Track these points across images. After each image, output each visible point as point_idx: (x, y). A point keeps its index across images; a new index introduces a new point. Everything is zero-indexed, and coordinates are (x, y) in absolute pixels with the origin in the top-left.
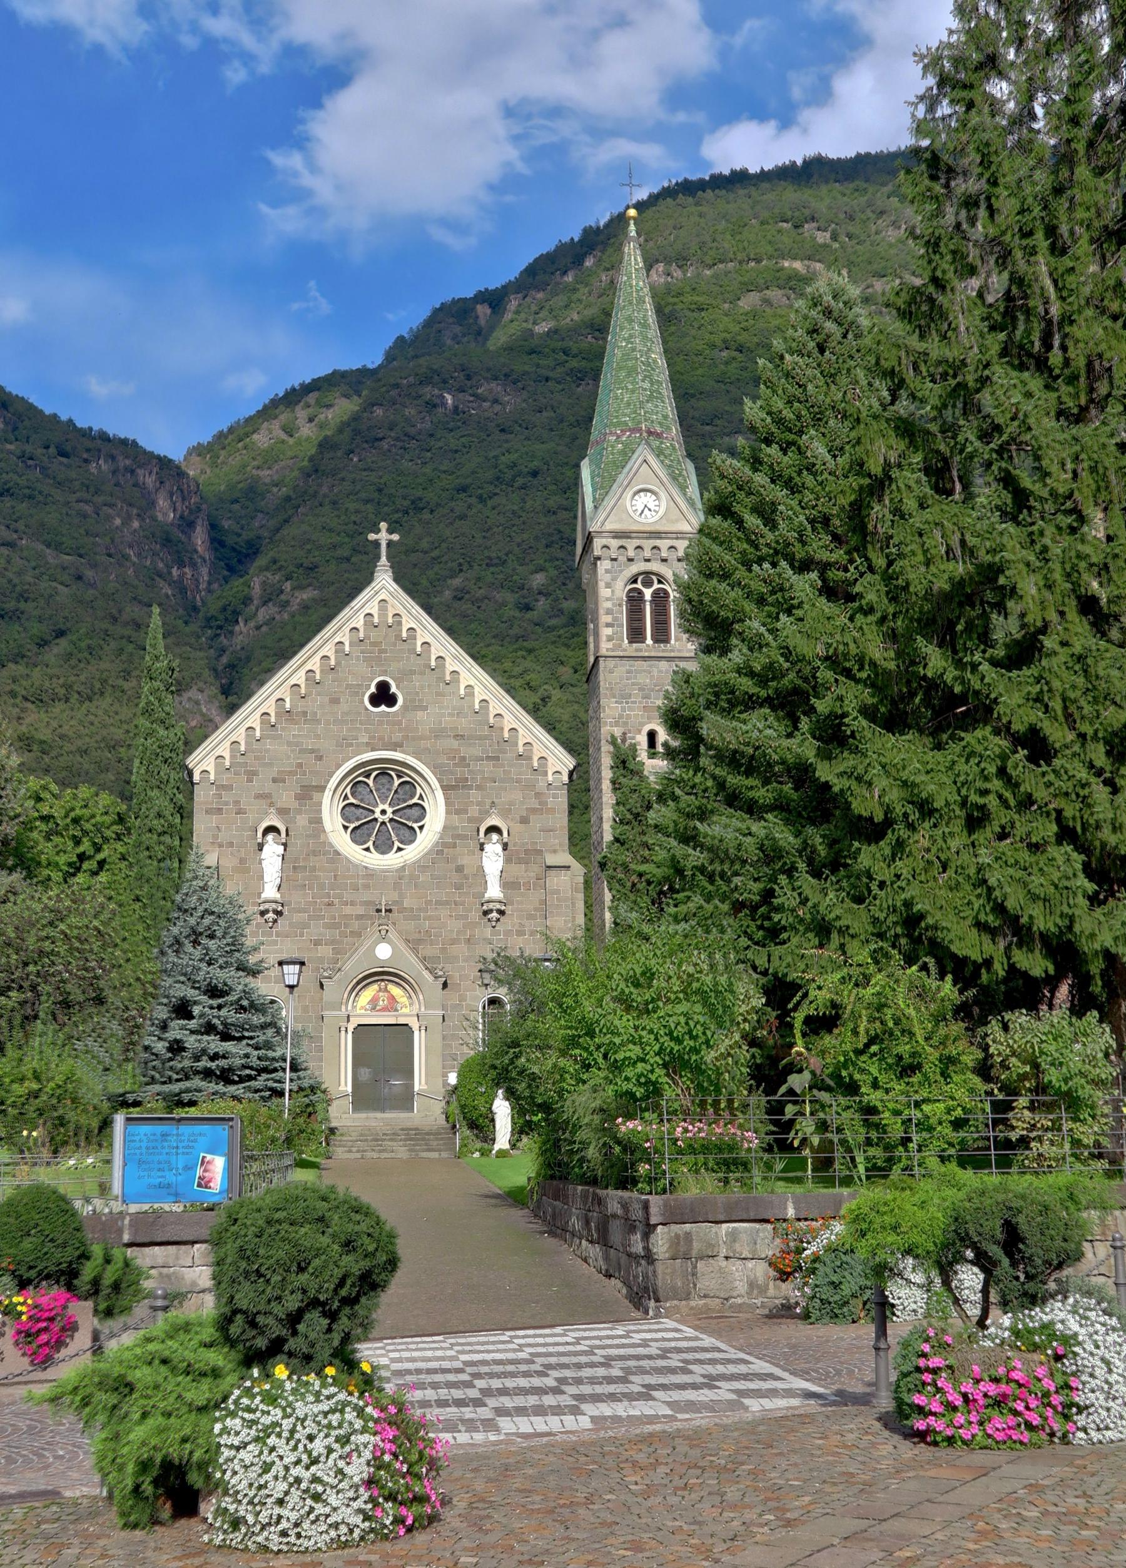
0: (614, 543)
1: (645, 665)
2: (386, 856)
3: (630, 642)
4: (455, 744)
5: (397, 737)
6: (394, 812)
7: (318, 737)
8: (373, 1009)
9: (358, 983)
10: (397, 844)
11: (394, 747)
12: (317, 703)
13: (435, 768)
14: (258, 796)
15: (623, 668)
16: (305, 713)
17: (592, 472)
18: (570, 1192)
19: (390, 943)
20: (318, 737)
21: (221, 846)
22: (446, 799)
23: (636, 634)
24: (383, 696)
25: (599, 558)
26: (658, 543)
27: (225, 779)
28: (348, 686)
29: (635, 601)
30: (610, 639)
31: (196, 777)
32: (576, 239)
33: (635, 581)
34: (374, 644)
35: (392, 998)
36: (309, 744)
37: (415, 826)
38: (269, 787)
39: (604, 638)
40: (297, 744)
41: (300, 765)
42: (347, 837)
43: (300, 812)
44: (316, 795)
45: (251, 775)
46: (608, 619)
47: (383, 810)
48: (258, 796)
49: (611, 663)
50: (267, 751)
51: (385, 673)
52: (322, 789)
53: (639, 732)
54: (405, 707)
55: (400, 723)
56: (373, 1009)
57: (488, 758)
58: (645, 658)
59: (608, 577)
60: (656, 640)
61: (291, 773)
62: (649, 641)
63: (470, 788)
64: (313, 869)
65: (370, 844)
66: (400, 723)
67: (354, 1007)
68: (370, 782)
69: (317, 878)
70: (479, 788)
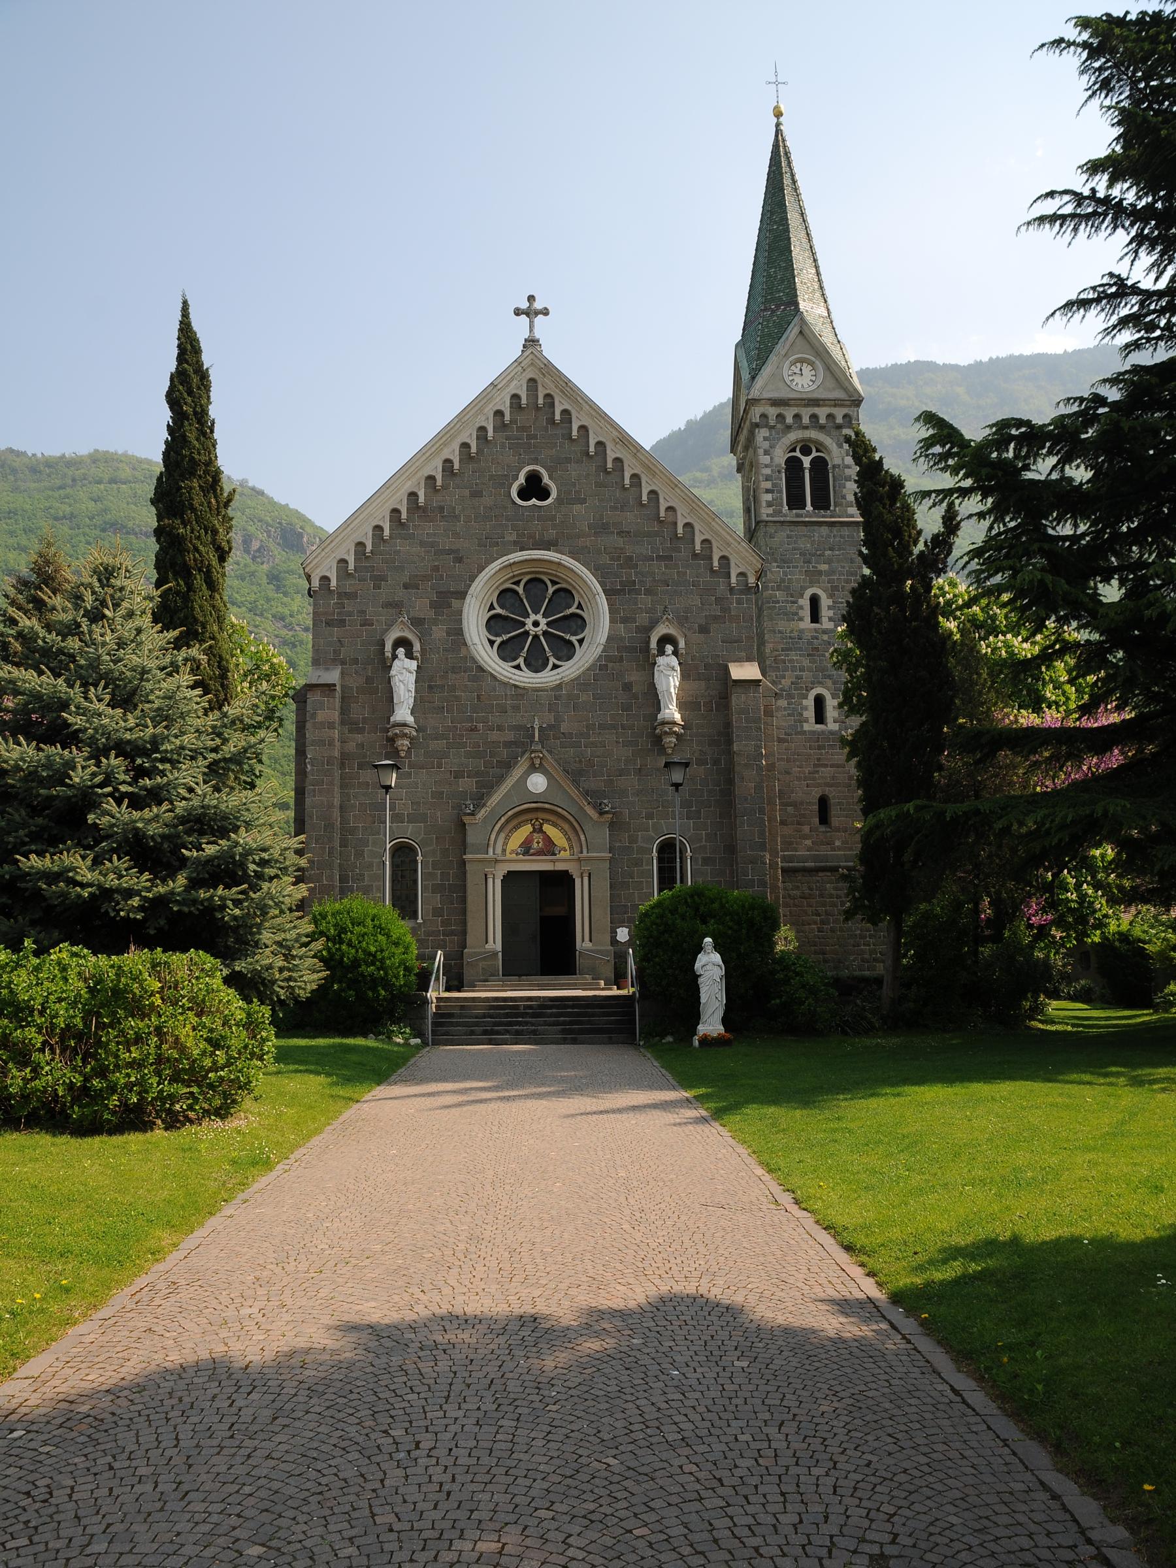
0: (772, 412)
1: (803, 530)
4: (620, 542)
5: (552, 533)
6: (548, 624)
7: (456, 535)
8: (526, 853)
9: (507, 821)
10: (552, 660)
13: (597, 570)
14: (388, 605)
15: (782, 535)
16: (441, 509)
19: (545, 772)
20: (456, 535)
21: (343, 663)
23: (796, 501)
24: (534, 488)
26: (816, 410)
27: (349, 586)
28: (491, 477)
29: (793, 466)
30: (769, 504)
33: (794, 450)
34: (522, 429)
35: (549, 841)
38: (400, 594)
40: (432, 545)
41: (436, 569)
43: (435, 622)
44: (455, 603)
45: (378, 580)
46: (768, 485)
47: (536, 623)
48: (388, 605)
51: (535, 461)
52: (462, 595)
53: (802, 596)
54: (558, 499)
55: (553, 518)
57: (659, 558)
58: (806, 524)
59: (766, 445)
61: (426, 578)
62: (809, 507)
63: (638, 592)
65: (521, 661)
66: (553, 518)
67: (504, 851)
68: (520, 590)
69: (458, 698)
70: (648, 592)
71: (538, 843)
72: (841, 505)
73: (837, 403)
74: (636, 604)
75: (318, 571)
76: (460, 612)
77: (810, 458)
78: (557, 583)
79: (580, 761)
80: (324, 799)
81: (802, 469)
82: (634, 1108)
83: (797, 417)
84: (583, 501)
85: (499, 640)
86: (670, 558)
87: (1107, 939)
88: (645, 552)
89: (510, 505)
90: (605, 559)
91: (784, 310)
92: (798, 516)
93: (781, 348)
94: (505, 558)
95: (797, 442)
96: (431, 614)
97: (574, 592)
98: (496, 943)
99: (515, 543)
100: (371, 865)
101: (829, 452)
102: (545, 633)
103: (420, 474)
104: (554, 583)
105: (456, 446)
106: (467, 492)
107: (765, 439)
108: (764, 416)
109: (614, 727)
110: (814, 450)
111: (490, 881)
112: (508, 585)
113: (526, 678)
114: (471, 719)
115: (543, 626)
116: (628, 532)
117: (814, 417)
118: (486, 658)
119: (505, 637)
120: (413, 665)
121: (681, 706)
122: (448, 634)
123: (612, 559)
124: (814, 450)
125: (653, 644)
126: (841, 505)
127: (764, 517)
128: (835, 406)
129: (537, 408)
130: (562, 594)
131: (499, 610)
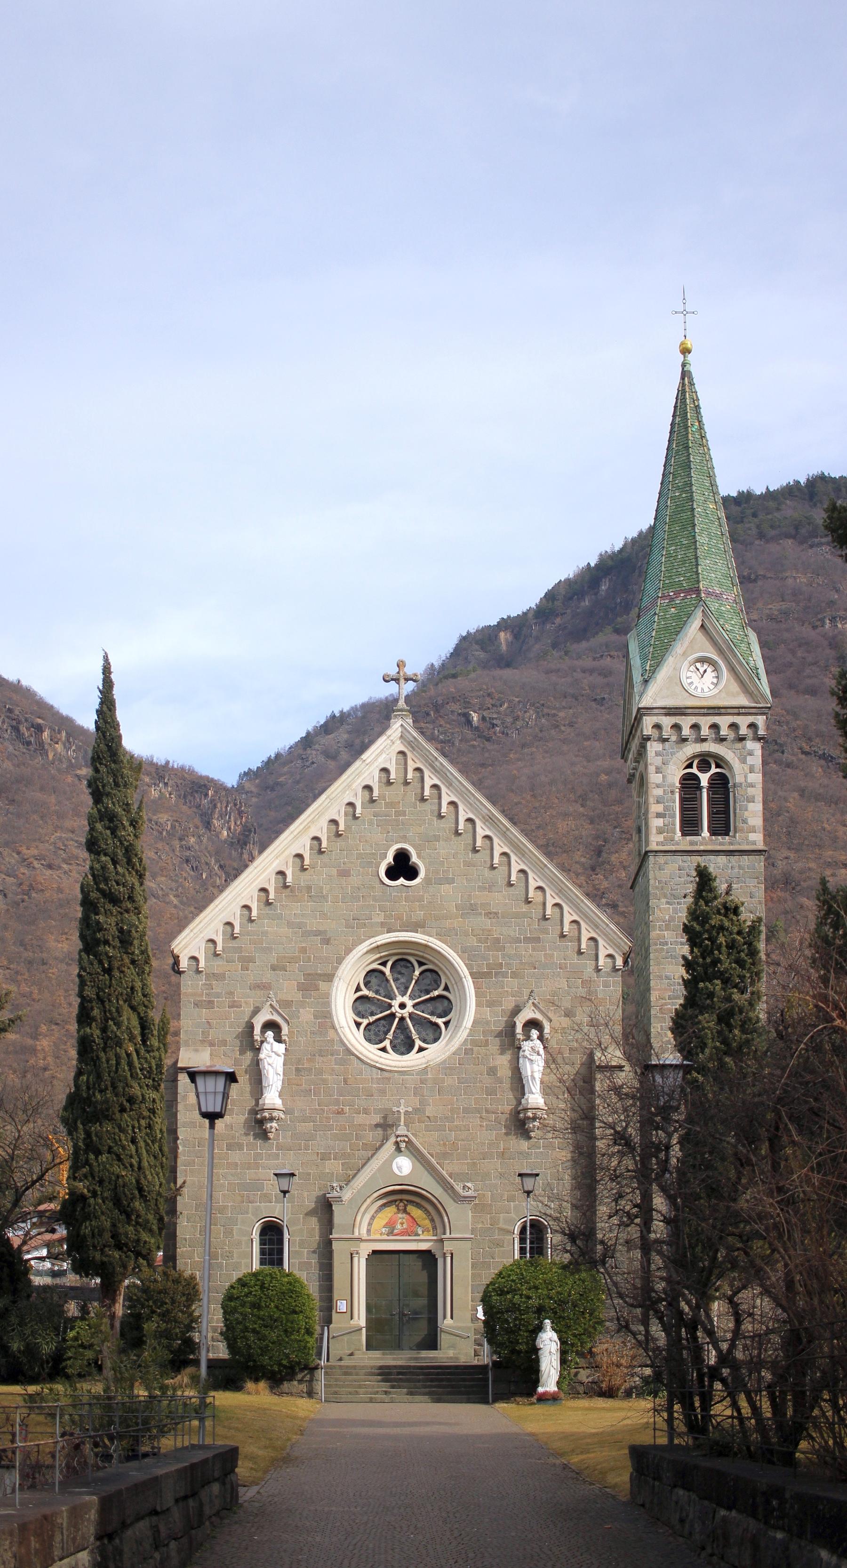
0: (667, 722)
2: (406, 1057)
3: (684, 834)
4: (487, 923)
7: (324, 916)
8: (391, 1233)
11: (415, 927)
12: (322, 876)
13: (465, 953)
16: (309, 888)
17: (642, 649)
18: (48, 1280)
20: (324, 916)
21: (212, 1045)
22: (477, 988)
23: (690, 825)
24: (402, 867)
25: (648, 739)
26: (716, 719)
27: (218, 966)
28: (359, 856)
29: (689, 783)
30: (660, 831)
31: (184, 964)
32: (592, 565)
36: (313, 924)
37: (440, 1021)
38: (268, 976)
39: (653, 831)
40: (300, 926)
41: (303, 950)
42: (360, 1035)
43: (302, 1004)
44: (322, 985)
46: (660, 808)
49: (661, 859)
50: (265, 933)
51: (404, 839)
52: (329, 978)
54: (427, 880)
55: (421, 899)
56: (391, 1233)
57: (527, 940)
59: (658, 761)
60: (713, 832)
61: (293, 960)
62: (706, 833)
63: (505, 975)
64: (320, 1072)
65: (387, 1043)
66: (421, 899)
68: (387, 970)
69: (325, 1081)
70: (515, 975)
71: (402, 1224)
72: (742, 831)
73: (739, 711)
74: (503, 987)
75: (186, 951)
76: (327, 996)
77: (709, 774)
78: (424, 964)
79: (445, 1144)
80: (196, 1179)
81: (699, 788)
82: (428, 1424)
83: (695, 727)
84: (451, 881)
85: (365, 1022)
86: (537, 940)
87: (657, 1376)
88: (512, 934)
89: (378, 885)
90: (473, 941)
91: (685, 598)
92: (692, 843)
93: (679, 648)
94: (372, 940)
95: (694, 757)
96: (299, 996)
97: (440, 973)
98: (361, 1319)
99: (382, 924)
100: (239, 1243)
101: (730, 768)
102: (411, 1015)
103: (286, 853)
104: (421, 964)
105: (324, 823)
106: (334, 872)
107: (657, 754)
108: (658, 727)
109: (478, 1111)
110: (713, 766)
111: (356, 1260)
112: (375, 966)
113: (392, 1060)
114: (337, 1102)
115: (409, 1008)
116: (495, 913)
117: (715, 727)
118: (353, 1041)
119: (371, 994)
120: (280, 1048)
121: (546, 1089)
122: (316, 1017)
123: (479, 941)
124: (713, 766)
125: (519, 1029)
126: (742, 831)
127: (653, 846)
128: (739, 714)
129: (406, 783)
130: (428, 974)
131: (365, 992)
